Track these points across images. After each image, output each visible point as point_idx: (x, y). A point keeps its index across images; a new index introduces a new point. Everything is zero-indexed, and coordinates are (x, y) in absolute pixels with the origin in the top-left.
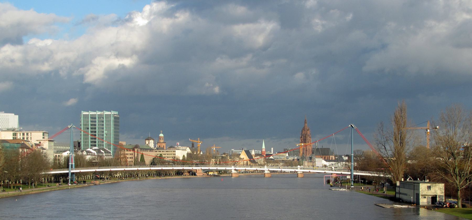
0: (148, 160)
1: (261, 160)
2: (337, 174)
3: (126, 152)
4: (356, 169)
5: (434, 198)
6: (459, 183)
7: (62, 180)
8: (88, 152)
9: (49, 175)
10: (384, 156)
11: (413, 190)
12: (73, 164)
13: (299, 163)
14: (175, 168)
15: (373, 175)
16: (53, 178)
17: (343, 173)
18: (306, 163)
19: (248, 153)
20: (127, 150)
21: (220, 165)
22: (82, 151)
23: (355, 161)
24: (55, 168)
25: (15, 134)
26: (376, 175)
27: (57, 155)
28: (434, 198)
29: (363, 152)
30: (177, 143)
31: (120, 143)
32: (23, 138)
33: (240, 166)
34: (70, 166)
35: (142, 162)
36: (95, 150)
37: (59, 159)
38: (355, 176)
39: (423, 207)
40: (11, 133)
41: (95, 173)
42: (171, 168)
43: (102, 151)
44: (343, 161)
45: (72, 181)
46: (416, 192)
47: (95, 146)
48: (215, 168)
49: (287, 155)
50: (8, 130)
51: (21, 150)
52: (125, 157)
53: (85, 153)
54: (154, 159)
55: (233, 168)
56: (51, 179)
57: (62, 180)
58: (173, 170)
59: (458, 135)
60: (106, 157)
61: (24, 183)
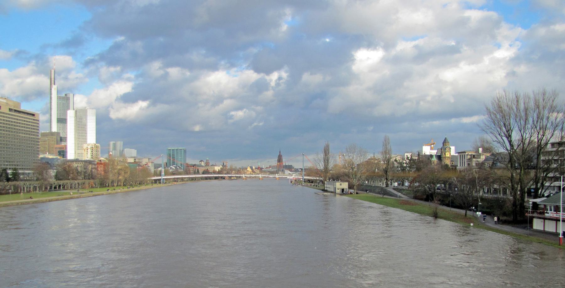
0: (201, 171)
1: (258, 171)
2: (296, 178)
3: (190, 168)
4: (305, 175)
5: (343, 190)
6: (355, 182)
7: (158, 182)
8: (171, 168)
9: (152, 180)
10: (319, 169)
11: (333, 186)
12: (164, 174)
13: (277, 172)
14: (214, 176)
15: (314, 178)
16: (154, 181)
17: (299, 177)
18: (280, 173)
19: (251, 168)
20: (190, 167)
21: (237, 174)
22: (168, 168)
23: (304, 172)
24: (154, 176)
25: (135, 159)
26: (315, 178)
27: (156, 169)
28: (343, 190)
29: (309, 167)
30: (112, 143)
31: (42, 158)
32: (139, 161)
33: (247, 175)
34: (162, 175)
35: (198, 173)
36: (174, 167)
37: (156, 172)
38: (305, 179)
39: (338, 194)
40: (133, 159)
41: (174, 178)
42: (213, 176)
43: (178, 167)
44: (299, 171)
45: (163, 182)
46: (334, 187)
47: (174, 165)
48: (235, 175)
49: (271, 169)
50: (132, 157)
51: (138, 167)
52: (189, 170)
53: (169, 168)
54: (204, 171)
55: (244, 175)
56: (153, 182)
57: (158, 182)
58: (213, 176)
59: (354, 159)
60: (180, 170)
61: (139, 184)
